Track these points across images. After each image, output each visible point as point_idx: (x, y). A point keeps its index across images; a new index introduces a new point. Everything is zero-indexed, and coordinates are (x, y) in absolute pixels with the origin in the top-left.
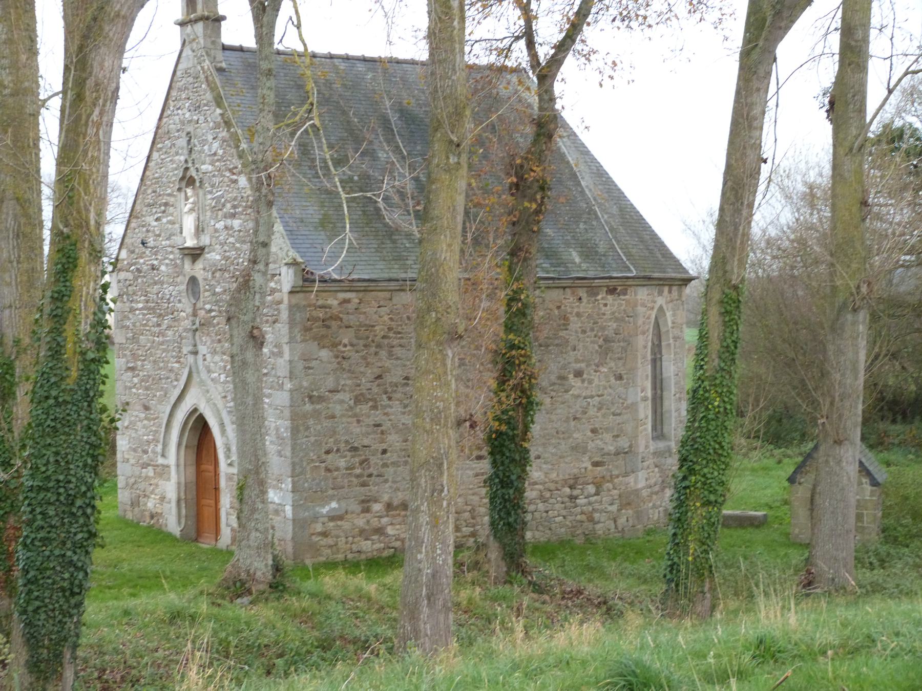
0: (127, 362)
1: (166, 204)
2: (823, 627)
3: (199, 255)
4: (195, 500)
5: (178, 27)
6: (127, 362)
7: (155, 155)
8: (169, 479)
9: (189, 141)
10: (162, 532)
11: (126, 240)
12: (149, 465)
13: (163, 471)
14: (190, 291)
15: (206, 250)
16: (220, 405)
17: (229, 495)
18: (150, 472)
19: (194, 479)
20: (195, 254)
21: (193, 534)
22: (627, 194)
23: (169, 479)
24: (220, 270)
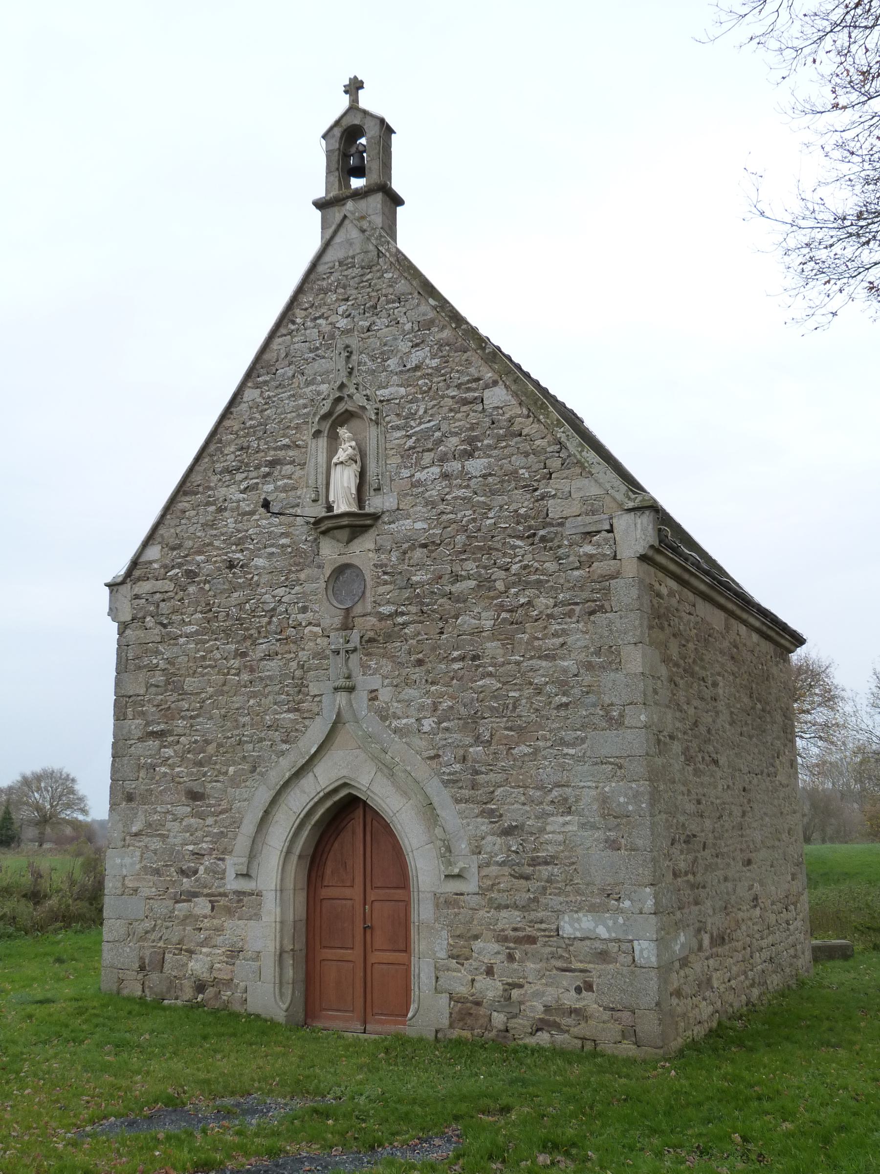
0: (148, 724)
1: (272, 464)
2: (86, 1021)
3: (365, 528)
4: (304, 952)
5: (318, 214)
6: (148, 724)
7: (251, 394)
8: (257, 916)
9: (348, 357)
10: (236, 1016)
11: (161, 531)
12: (196, 895)
13: (243, 903)
14: (330, 592)
15: (386, 519)
16: (422, 770)
17: (444, 933)
18: (202, 906)
19: (304, 916)
20: (358, 524)
21: (301, 1016)
22: (789, 624)
23: (257, 916)
24: (424, 546)
